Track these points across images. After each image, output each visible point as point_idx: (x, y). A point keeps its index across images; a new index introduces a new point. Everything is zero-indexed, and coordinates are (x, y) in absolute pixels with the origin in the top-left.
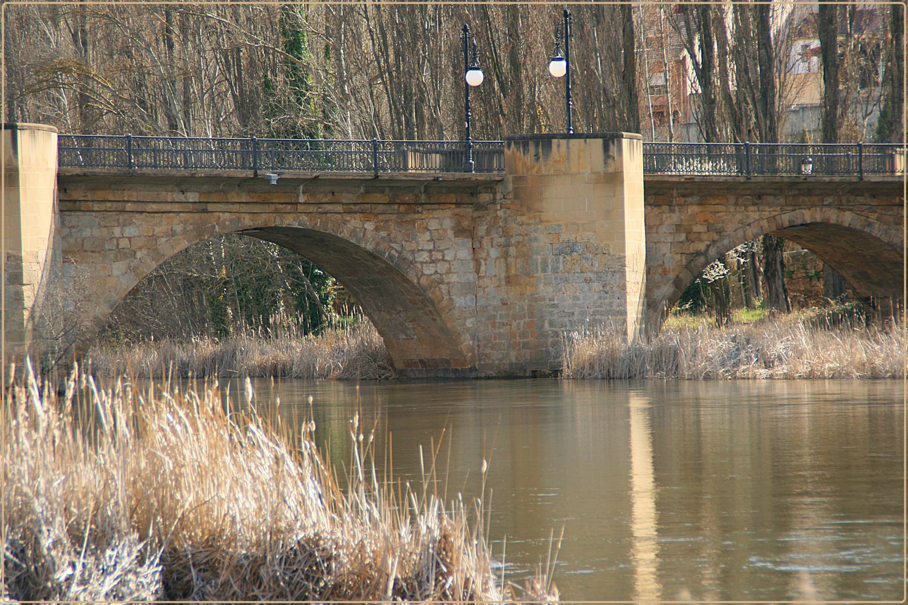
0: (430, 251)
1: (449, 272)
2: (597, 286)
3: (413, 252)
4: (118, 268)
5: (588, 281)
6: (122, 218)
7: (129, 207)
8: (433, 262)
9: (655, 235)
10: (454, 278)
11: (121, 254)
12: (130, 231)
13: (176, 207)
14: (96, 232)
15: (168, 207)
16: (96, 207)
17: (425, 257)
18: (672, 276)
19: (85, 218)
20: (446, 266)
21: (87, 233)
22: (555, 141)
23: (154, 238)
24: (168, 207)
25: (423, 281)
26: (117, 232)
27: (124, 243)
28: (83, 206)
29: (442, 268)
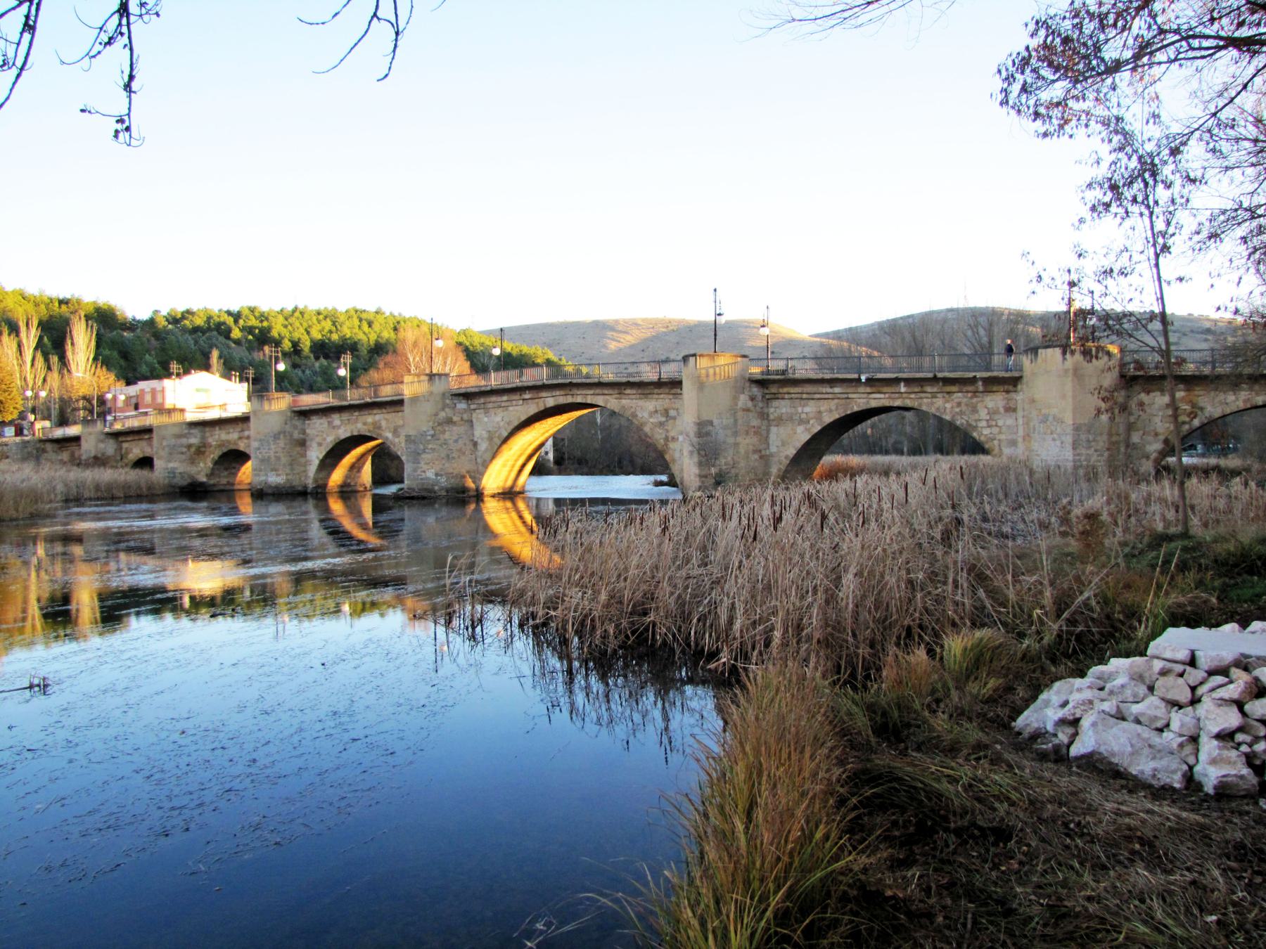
0: (987, 421)
1: (1000, 433)
2: (1058, 443)
3: (976, 421)
4: (800, 429)
5: (1054, 440)
6: (802, 402)
7: (804, 396)
8: (989, 426)
9: (689, 407)
10: (1003, 437)
11: (801, 422)
12: (807, 409)
13: (830, 396)
14: (789, 410)
15: (826, 396)
16: (786, 396)
17: (984, 424)
18: (1162, 437)
19: (783, 402)
20: (998, 429)
21: (784, 410)
22: (1040, 351)
23: (820, 412)
24: (826, 396)
25: (982, 438)
26: (800, 410)
27: (803, 416)
28: (780, 396)
29: (995, 430)
